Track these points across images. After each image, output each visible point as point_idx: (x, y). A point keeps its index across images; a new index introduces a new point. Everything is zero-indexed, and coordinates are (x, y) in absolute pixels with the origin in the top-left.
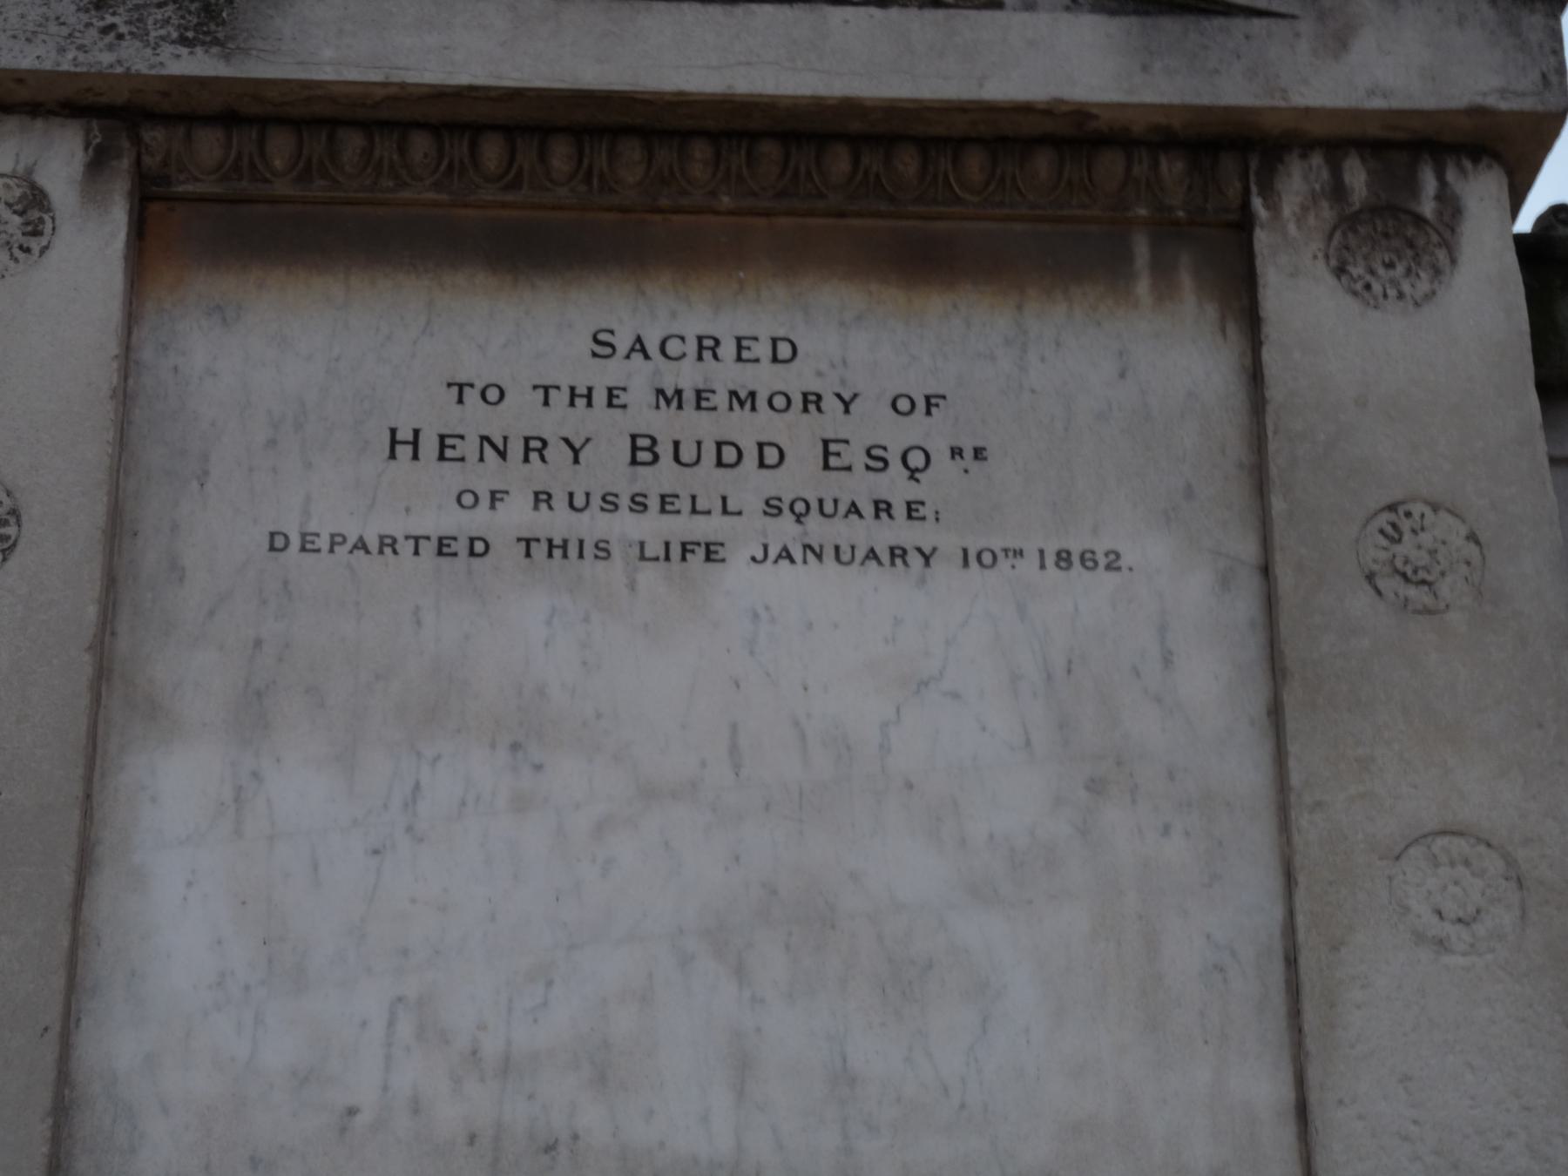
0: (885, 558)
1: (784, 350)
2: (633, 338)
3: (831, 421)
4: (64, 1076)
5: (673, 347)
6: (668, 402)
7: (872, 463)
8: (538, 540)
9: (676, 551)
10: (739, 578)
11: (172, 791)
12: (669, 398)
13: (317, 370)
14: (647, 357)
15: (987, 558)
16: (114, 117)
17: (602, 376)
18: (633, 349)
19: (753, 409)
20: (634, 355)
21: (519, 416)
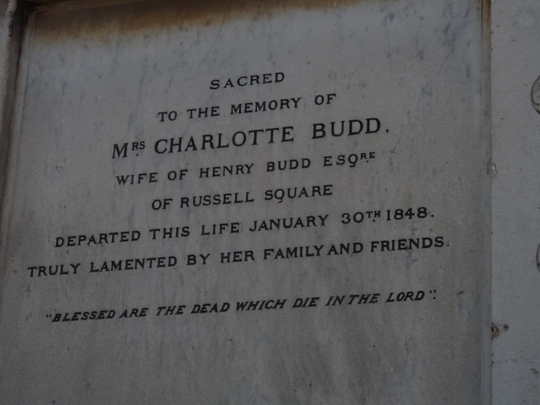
0: (305, 223)
1: (280, 77)
2: (228, 80)
5: (242, 82)
6: (236, 110)
7: (213, 86)
8: (159, 230)
9: (218, 230)
14: (232, 86)
15: (359, 217)
18: (227, 84)
19: (264, 110)
20: (227, 86)
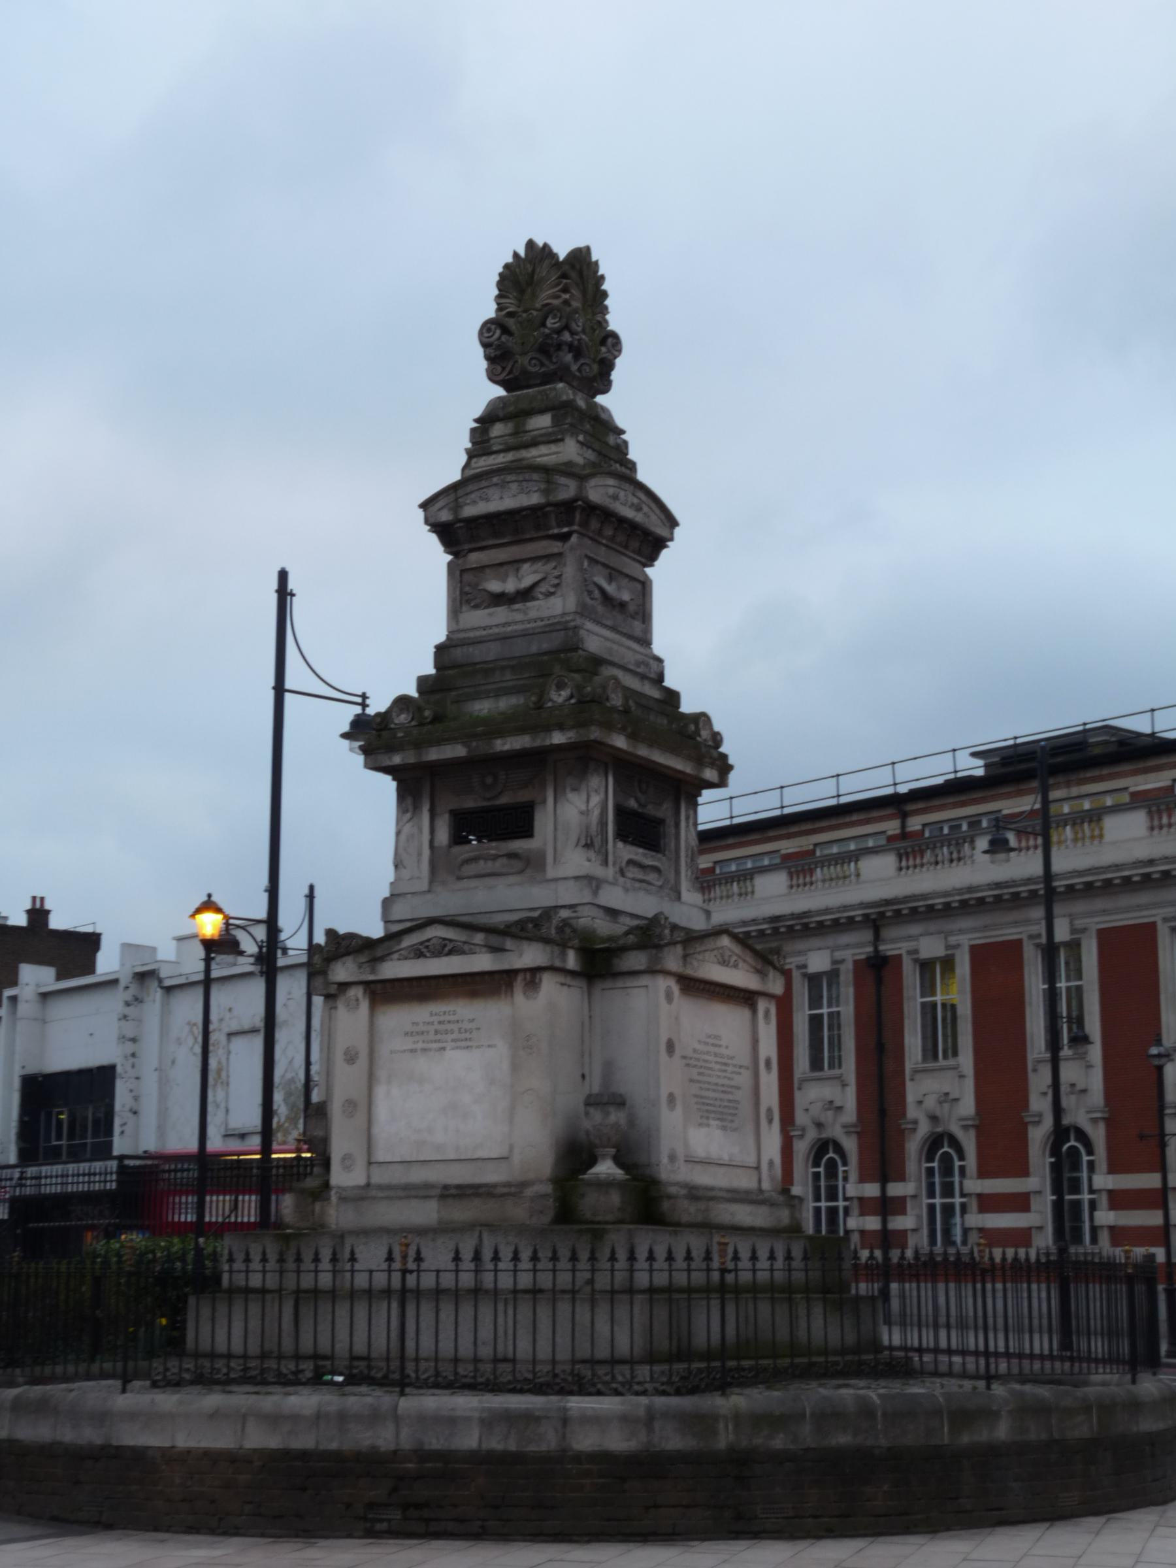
3: (460, 1025)
4: (263, 1320)
10: (449, 1054)
11: (380, 1091)
12: (440, 1023)
13: (399, 1019)
16: (366, 984)
17: (432, 1019)
21: (421, 1028)
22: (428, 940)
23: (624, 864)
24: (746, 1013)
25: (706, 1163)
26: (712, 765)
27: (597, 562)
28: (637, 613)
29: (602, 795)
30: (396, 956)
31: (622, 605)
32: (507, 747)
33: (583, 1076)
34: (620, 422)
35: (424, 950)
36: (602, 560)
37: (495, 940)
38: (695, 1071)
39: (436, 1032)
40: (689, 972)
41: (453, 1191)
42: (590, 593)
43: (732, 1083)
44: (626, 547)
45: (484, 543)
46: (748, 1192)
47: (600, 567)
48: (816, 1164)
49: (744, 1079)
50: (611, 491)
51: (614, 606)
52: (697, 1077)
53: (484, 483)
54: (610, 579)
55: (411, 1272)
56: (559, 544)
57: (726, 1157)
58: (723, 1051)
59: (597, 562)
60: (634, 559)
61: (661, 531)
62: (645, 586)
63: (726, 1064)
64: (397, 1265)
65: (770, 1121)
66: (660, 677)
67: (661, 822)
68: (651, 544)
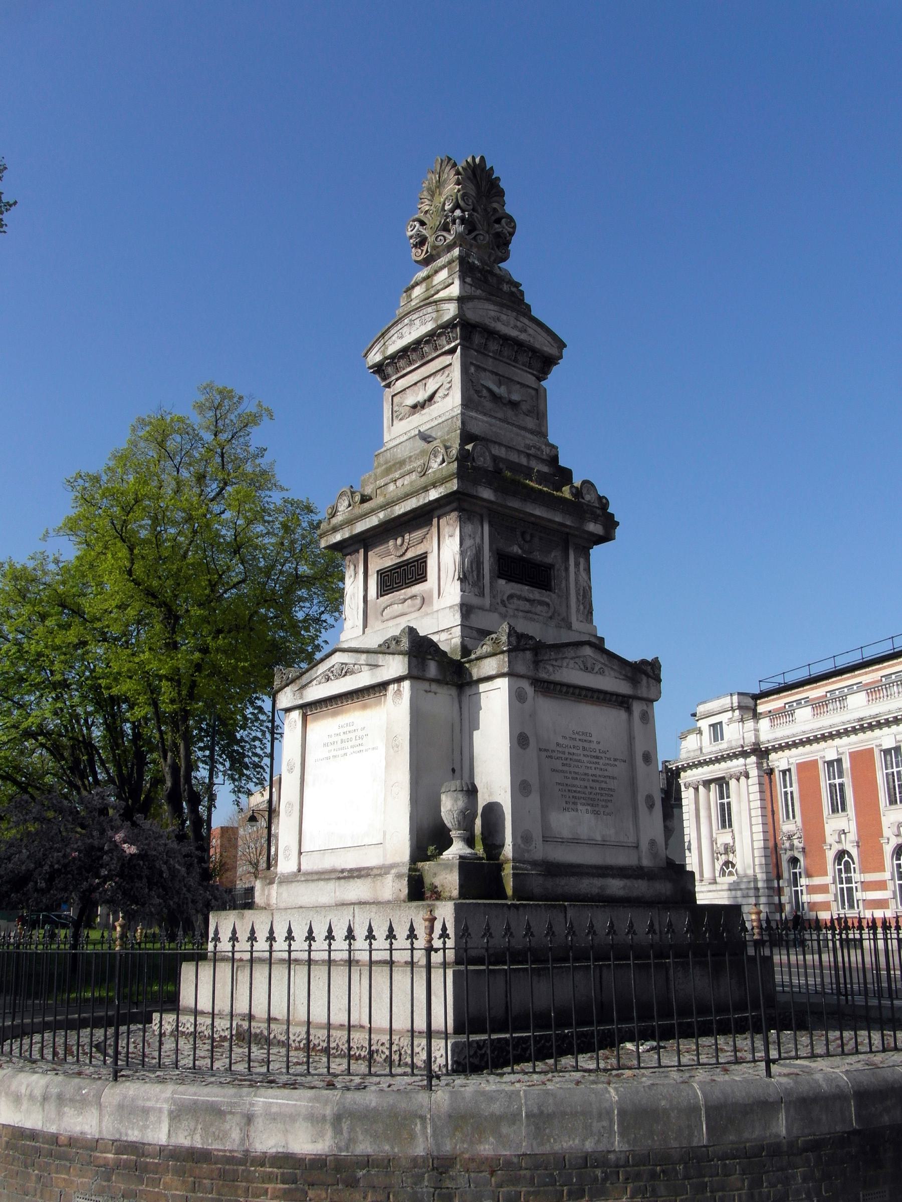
3: (356, 734)
22: (333, 666)
23: (505, 598)
24: (623, 714)
25: (575, 841)
26: (595, 519)
27: (485, 370)
28: (529, 411)
29: (478, 540)
30: (314, 682)
31: (514, 405)
32: (402, 511)
33: (453, 770)
34: (516, 278)
35: (331, 675)
36: (490, 368)
37: (373, 659)
38: (559, 762)
39: (342, 741)
40: (543, 675)
41: (345, 874)
42: (477, 392)
43: (606, 773)
44: (516, 360)
45: (405, 371)
46: (630, 868)
47: (488, 373)
48: (839, 864)
49: (620, 770)
50: (493, 314)
51: (504, 404)
52: (561, 768)
53: (400, 326)
54: (500, 384)
55: (436, 950)
56: (450, 357)
57: (599, 838)
58: (594, 746)
59: (485, 370)
60: (527, 371)
61: (549, 349)
62: (539, 395)
63: (597, 757)
64: (421, 943)
65: (651, 806)
66: (555, 459)
67: (551, 567)
68: (545, 363)
